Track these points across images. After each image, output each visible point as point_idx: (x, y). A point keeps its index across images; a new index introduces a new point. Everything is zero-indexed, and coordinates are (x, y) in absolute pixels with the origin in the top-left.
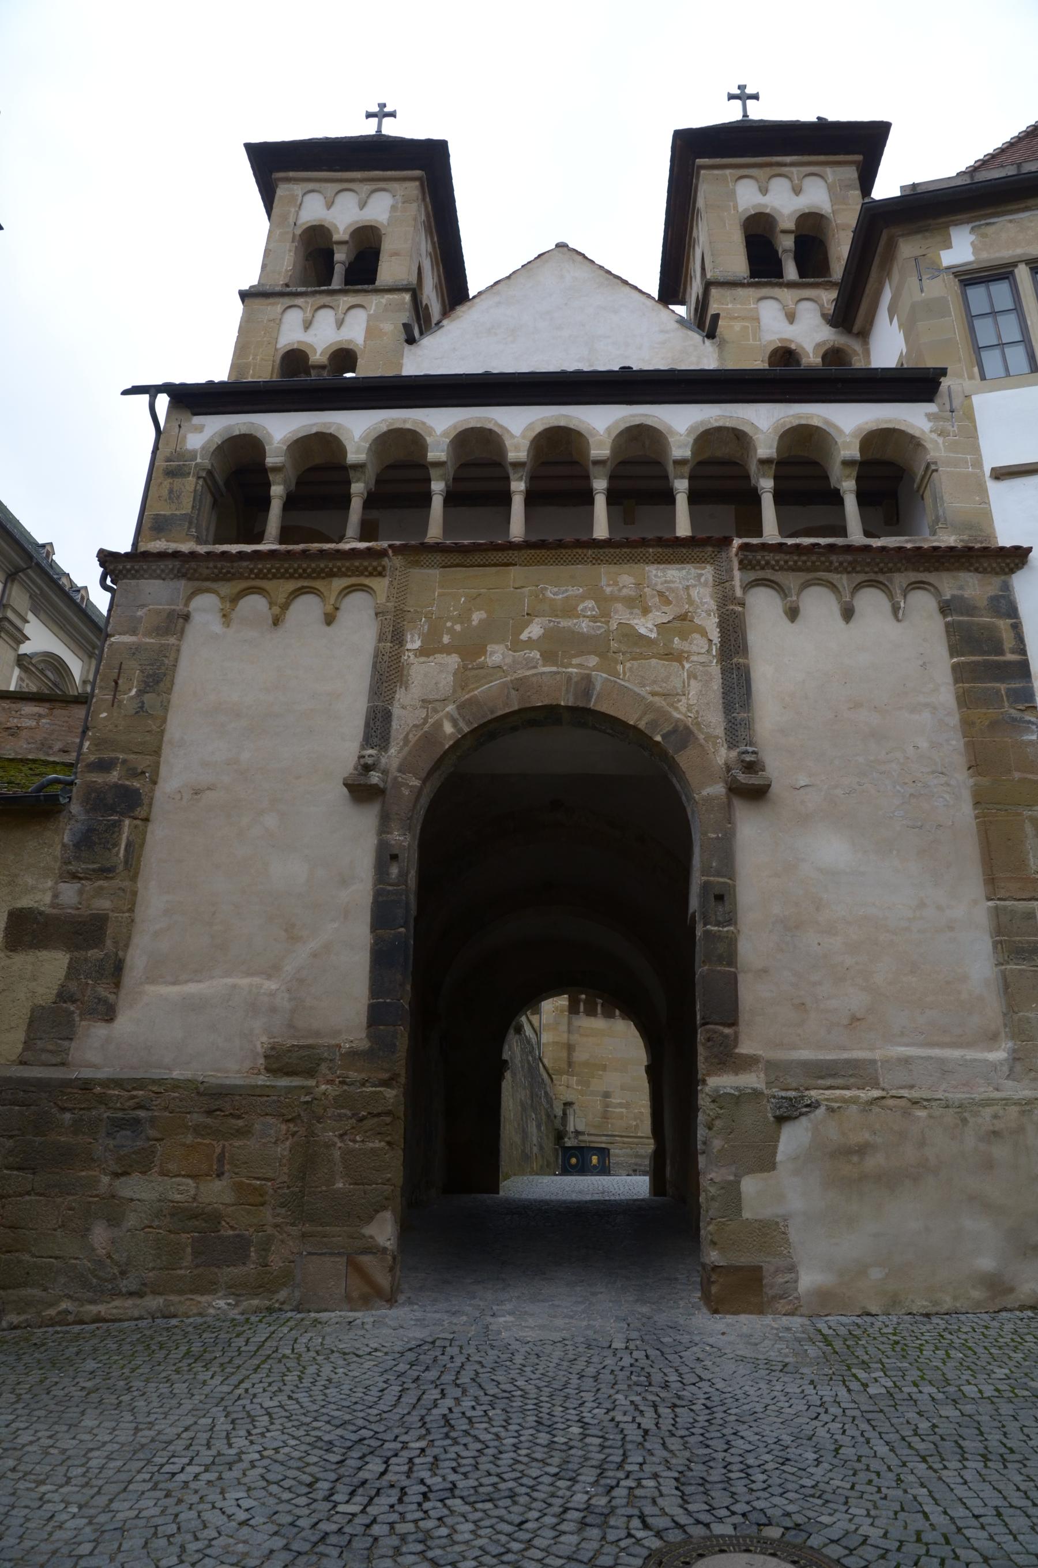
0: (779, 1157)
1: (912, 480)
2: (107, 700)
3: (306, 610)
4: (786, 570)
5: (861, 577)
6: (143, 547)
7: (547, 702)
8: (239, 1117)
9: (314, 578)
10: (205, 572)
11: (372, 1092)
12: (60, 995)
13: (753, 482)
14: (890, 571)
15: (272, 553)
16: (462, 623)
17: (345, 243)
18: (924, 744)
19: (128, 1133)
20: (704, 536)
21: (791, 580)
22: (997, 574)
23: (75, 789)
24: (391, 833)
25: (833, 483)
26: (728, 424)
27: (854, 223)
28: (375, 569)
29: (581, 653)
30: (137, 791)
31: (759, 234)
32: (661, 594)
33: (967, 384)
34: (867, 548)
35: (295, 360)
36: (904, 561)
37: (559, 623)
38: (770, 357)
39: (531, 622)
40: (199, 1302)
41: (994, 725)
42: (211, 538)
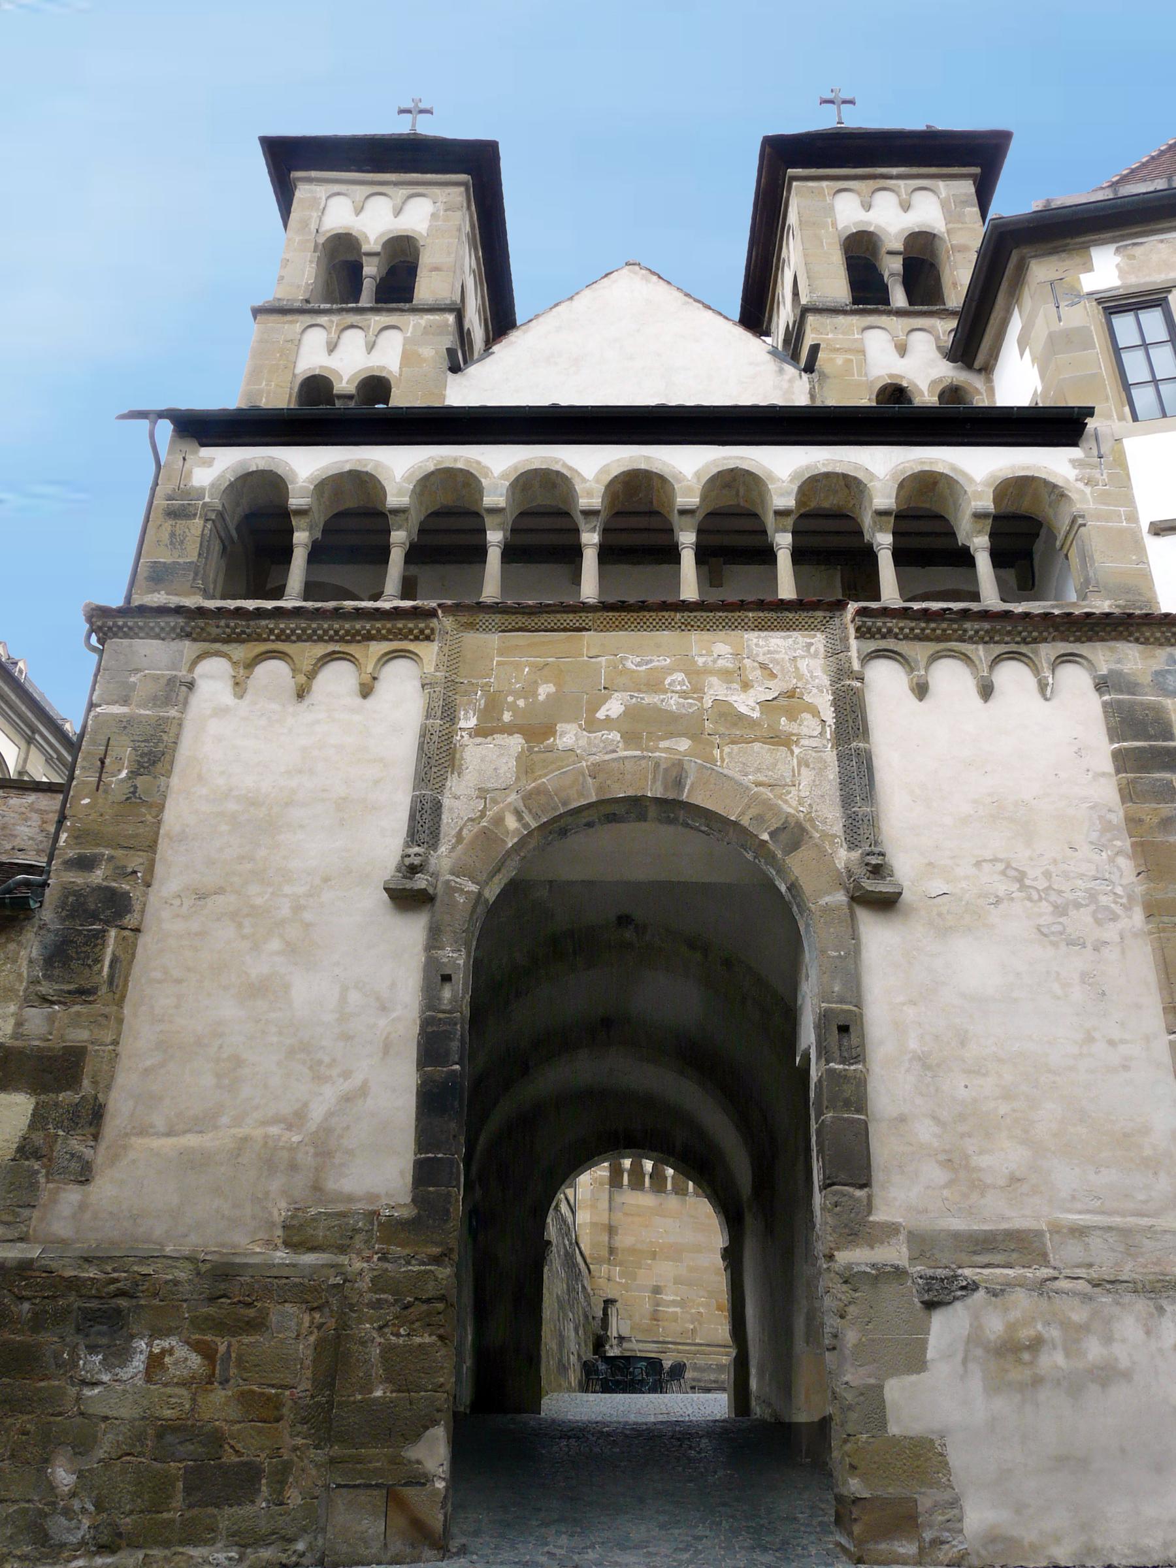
0: (930, 1355)
1: (1052, 536)
2: (88, 783)
3: (337, 680)
4: (912, 639)
5: (998, 649)
6: (137, 601)
7: (630, 792)
8: (249, 1305)
9: (347, 642)
10: (214, 631)
11: (420, 1272)
12: (21, 1149)
13: (867, 537)
14: (1035, 641)
15: (297, 612)
16: (526, 698)
17: (377, 254)
19: (104, 1328)
20: (814, 599)
21: (919, 651)
22: (1161, 645)
23: (47, 891)
24: (443, 949)
25: (962, 539)
26: (838, 470)
27: (977, 243)
28: (422, 632)
29: (670, 735)
30: (126, 896)
31: (860, 254)
32: (763, 666)
34: (1007, 615)
35: (316, 387)
36: (1051, 630)
37: (642, 699)
38: (877, 396)
39: (609, 697)
40: (192, 1557)
42: (218, 594)
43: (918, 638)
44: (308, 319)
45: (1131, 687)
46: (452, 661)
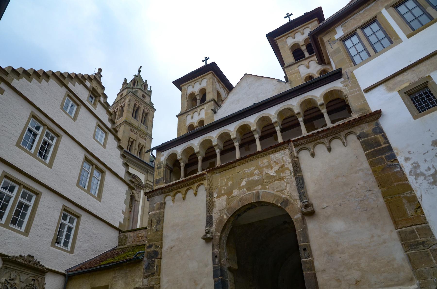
3: (191, 193)
5: (330, 138)
10: (167, 191)
14: (339, 132)
18: (362, 183)
21: (310, 146)
22: (373, 121)
29: (257, 186)
32: (275, 162)
33: (351, 69)
34: (333, 127)
35: (191, 127)
41: (383, 170)
43: (309, 142)
44: (187, 114)
45: (367, 135)
46: (211, 183)
